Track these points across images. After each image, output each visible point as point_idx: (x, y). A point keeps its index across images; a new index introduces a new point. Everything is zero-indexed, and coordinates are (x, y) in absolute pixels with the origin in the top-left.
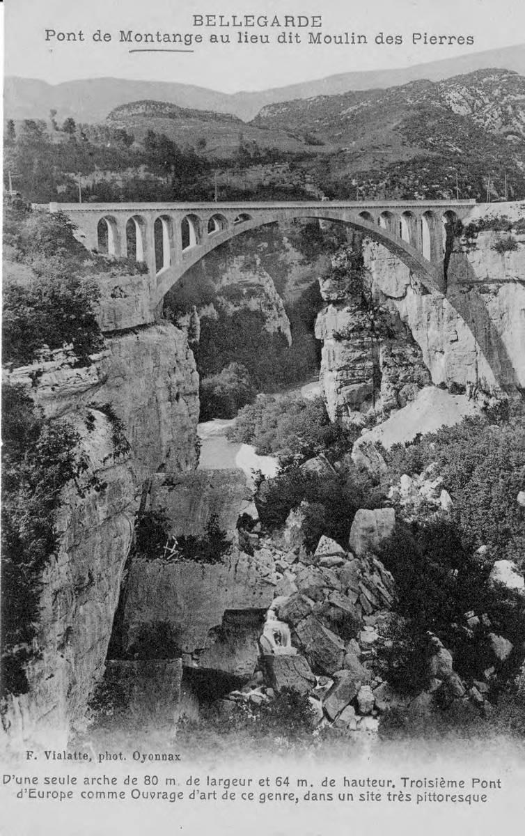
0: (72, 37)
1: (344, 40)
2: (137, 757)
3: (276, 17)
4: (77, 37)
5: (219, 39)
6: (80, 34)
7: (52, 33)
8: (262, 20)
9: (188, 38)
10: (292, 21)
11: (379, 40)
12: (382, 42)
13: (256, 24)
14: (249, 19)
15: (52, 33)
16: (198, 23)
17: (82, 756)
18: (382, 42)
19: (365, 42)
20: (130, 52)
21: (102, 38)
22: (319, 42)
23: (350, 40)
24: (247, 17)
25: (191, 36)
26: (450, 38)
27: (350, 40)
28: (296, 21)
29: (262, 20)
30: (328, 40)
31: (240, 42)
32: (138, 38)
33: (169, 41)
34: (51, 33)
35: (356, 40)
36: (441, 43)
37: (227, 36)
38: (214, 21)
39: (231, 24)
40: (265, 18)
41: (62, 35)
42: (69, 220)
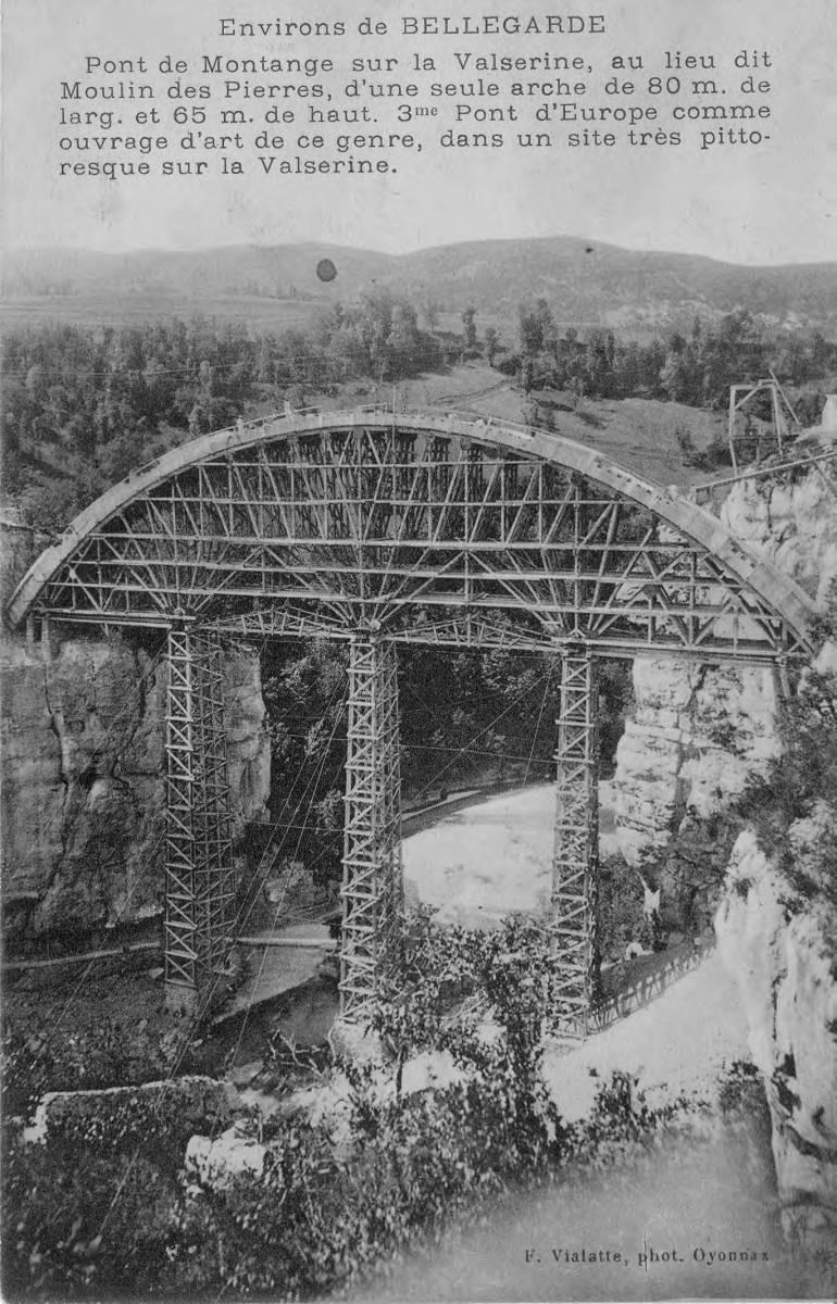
1: (117, 92)
3: (533, 19)
4: (506, 115)
5: (626, 62)
7: (466, 110)
8: (511, 24)
9: (145, 142)
10: (559, 24)
11: (747, 87)
13: (501, 28)
14: (490, 21)
16: (409, 29)
18: (632, 110)
19: (548, 144)
23: (127, 93)
24: (486, 19)
26: (286, 88)
27: (127, 93)
28: (566, 25)
29: (511, 24)
31: (226, 172)
32: (91, 93)
34: (465, 110)
35: (137, 93)
37: (711, 58)
38: (434, 26)
39: (482, 29)
40: (516, 20)
41: (674, 82)
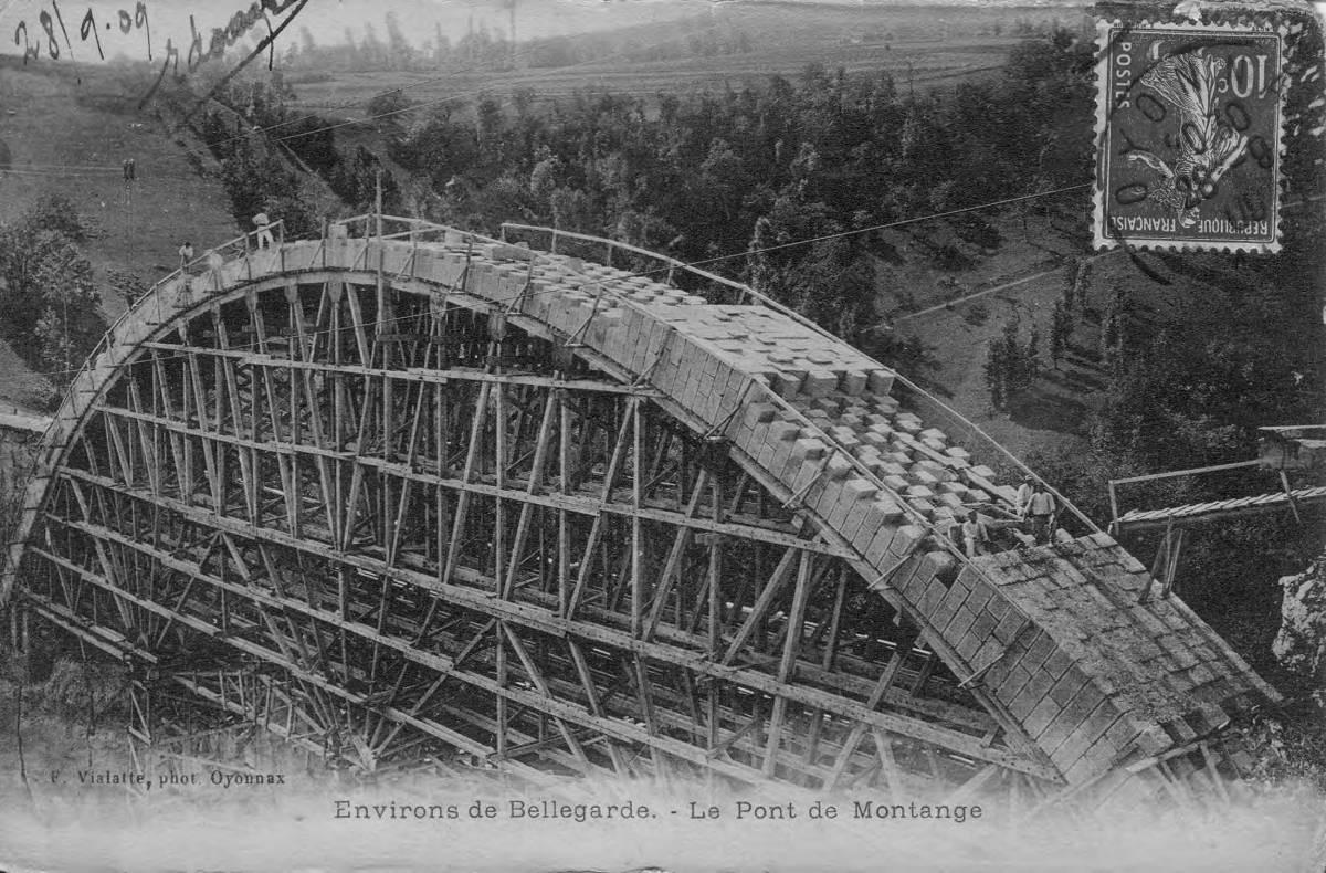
0: (777, 812)
2: (217, 778)
4: (786, 812)
6: (790, 808)
12: (631, 815)
15: (747, 807)
17: (135, 779)
20: (191, 17)
21: (483, 813)
22: (869, 816)
25: (964, 809)
30: (882, 812)
31: (857, 816)
33: (600, 816)
36: (403, 817)
42: (1144, 773)
